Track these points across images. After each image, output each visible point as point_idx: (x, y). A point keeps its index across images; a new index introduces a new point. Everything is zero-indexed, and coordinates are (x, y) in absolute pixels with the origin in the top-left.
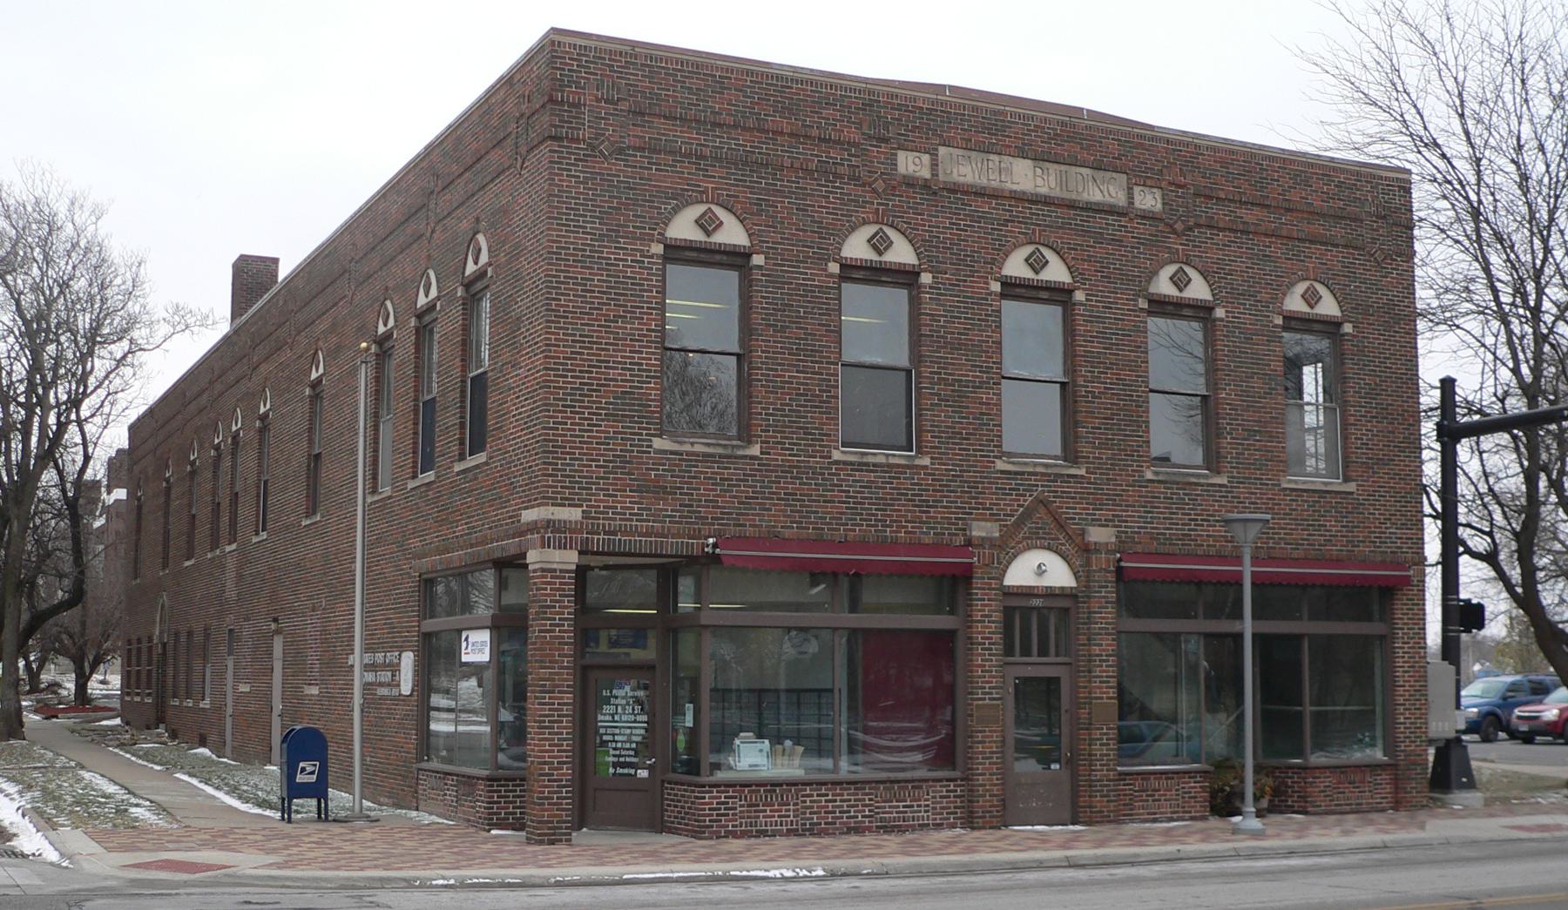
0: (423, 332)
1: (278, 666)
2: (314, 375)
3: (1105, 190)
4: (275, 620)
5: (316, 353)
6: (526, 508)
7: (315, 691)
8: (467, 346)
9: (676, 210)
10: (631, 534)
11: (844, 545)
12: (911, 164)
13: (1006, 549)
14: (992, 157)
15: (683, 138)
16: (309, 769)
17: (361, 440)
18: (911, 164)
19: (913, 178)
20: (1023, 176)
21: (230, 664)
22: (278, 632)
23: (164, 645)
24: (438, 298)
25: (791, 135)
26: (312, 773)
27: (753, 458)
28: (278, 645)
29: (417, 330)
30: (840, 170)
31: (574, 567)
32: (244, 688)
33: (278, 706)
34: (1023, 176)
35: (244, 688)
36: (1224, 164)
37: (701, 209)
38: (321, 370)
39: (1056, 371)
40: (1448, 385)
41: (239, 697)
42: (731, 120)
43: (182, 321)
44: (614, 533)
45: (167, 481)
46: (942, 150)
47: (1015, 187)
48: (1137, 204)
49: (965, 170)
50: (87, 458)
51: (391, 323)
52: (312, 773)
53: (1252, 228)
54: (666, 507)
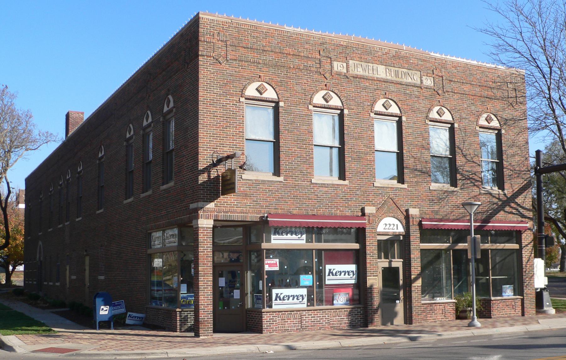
0: (145, 137)
1: (87, 268)
2: (100, 155)
3: (414, 78)
4: (86, 251)
5: (101, 147)
6: (192, 203)
7: (102, 278)
8: (164, 138)
9: (249, 84)
10: (234, 212)
11: (314, 216)
12: (339, 67)
13: (378, 218)
14: (370, 64)
15: (251, 56)
16: (106, 309)
17: (151, 145)
18: (339, 67)
19: (340, 73)
20: (381, 72)
21: (68, 268)
22: (87, 255)
23: (41, 262)
24: (152, 122)
25: (293, 55)
26: (106, 310)
27: (280, 182)
28: (87, 260)
29: (143, 135)
30: (312, 69)
31: (212, 226)
32: (74, 277)
33: (88, 284)
34: (381, 72)
35: (74, 277)
36: (455, 67)
37: (260, 83)
38: (103, 153)
39: (395, 148)
40: (538, 152)
41: (71, 281)
42: (269, 49)
43: (48, 137)
44: (227, 212)
45: (41, 199)
46: (351, 62)
47: (378, 76)
48: (424, 83)
49: (358, 68)
50: (9, 192)
51: (132, 133)
52: (106, 310)
53: (467, 93)
54: (248, 202)
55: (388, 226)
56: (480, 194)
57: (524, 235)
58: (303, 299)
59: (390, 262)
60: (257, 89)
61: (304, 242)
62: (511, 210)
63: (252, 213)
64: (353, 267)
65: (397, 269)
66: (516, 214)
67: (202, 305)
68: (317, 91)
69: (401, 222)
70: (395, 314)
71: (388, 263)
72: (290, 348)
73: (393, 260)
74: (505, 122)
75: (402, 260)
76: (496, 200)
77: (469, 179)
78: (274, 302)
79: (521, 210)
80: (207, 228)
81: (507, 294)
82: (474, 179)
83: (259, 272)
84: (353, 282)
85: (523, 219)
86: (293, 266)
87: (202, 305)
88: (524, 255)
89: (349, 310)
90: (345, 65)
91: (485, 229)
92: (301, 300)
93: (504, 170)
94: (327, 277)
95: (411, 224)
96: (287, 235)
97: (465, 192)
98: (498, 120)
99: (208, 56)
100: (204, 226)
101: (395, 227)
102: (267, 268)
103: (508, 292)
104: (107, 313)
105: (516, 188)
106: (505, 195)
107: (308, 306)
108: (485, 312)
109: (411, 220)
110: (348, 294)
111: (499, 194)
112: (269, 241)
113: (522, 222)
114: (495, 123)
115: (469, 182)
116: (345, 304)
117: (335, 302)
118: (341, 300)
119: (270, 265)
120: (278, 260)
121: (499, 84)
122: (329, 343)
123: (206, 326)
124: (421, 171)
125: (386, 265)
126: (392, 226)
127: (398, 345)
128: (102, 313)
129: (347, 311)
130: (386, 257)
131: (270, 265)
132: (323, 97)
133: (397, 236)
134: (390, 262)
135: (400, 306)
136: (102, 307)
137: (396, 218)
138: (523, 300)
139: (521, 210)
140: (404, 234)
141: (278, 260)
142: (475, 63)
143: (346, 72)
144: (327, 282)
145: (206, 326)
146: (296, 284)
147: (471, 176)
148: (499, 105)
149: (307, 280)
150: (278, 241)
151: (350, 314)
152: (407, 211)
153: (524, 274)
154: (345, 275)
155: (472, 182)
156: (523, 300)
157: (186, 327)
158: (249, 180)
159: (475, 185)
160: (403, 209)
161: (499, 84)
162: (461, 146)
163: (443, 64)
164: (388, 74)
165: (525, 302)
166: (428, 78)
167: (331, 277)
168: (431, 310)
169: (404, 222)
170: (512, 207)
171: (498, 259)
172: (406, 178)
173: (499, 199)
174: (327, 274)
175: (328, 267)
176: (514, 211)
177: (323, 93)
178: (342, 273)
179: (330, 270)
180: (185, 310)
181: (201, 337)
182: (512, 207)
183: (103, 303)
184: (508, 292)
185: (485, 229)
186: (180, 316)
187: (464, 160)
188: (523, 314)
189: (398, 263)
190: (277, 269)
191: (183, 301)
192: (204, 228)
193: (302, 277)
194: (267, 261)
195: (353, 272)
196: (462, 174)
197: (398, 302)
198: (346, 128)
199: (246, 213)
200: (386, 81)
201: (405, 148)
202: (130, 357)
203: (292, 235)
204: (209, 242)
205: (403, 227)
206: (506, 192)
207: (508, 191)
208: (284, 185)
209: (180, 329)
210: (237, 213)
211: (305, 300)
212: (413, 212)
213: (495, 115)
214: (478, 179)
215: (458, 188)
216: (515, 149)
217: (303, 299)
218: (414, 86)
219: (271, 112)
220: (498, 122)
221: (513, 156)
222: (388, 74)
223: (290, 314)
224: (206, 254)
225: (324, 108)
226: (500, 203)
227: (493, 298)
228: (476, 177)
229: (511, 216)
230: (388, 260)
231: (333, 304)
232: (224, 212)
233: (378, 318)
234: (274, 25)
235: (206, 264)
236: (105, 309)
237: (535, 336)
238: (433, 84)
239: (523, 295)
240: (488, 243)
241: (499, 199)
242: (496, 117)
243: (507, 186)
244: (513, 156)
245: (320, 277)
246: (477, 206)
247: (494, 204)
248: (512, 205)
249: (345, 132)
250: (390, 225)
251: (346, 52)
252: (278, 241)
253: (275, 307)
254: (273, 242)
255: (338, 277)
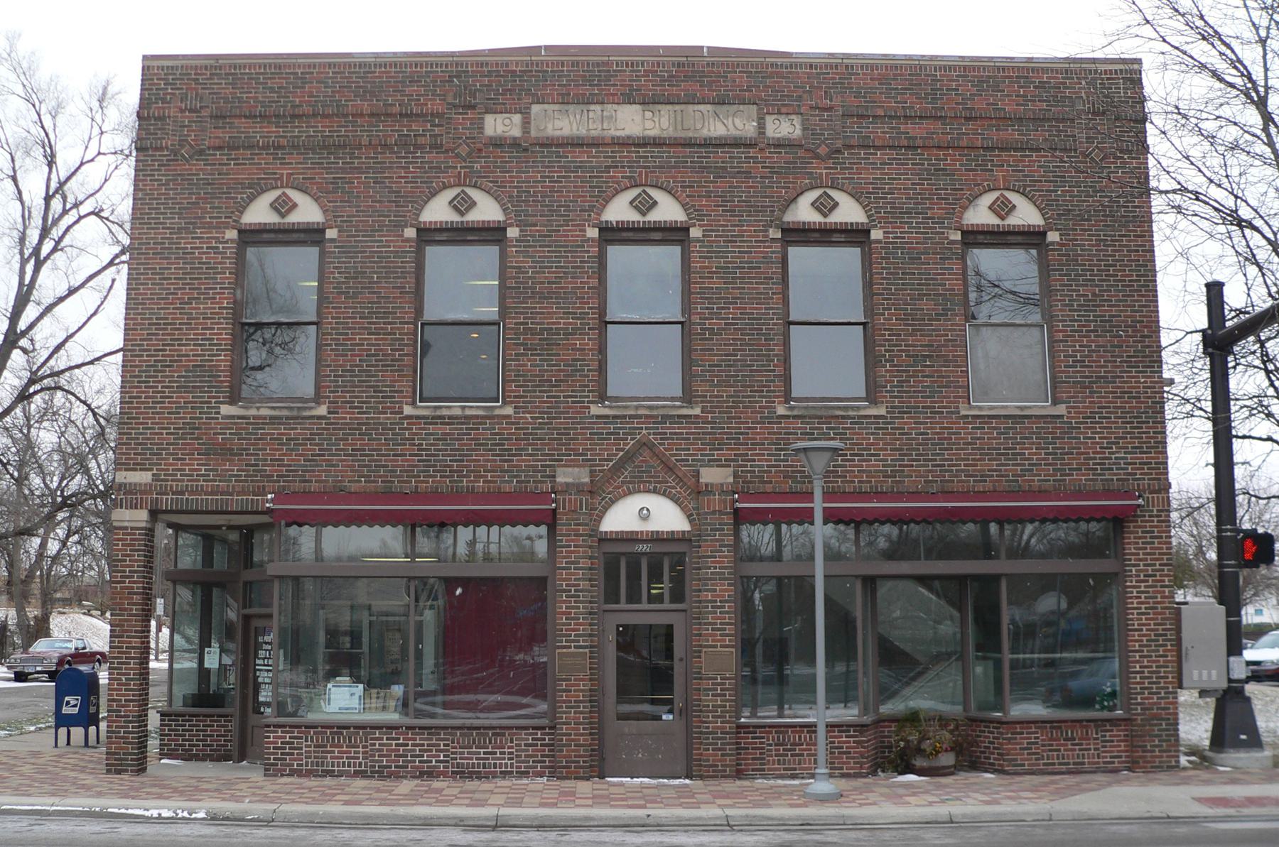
12: (498, 125)
16: (73, 703)
18: (498, 125)
20: (630, 121)
26: (75, 706)
34: (630, 121)
44: (182, 493)
52: (75, 706)
63: (242, 493)
80: (132, 528)
100: (126, 524)
127: (467, 801)
192: (126, 528)
202: (53, 829)
204: (136, 561)
224: (127, 588)
235: (125, 610)
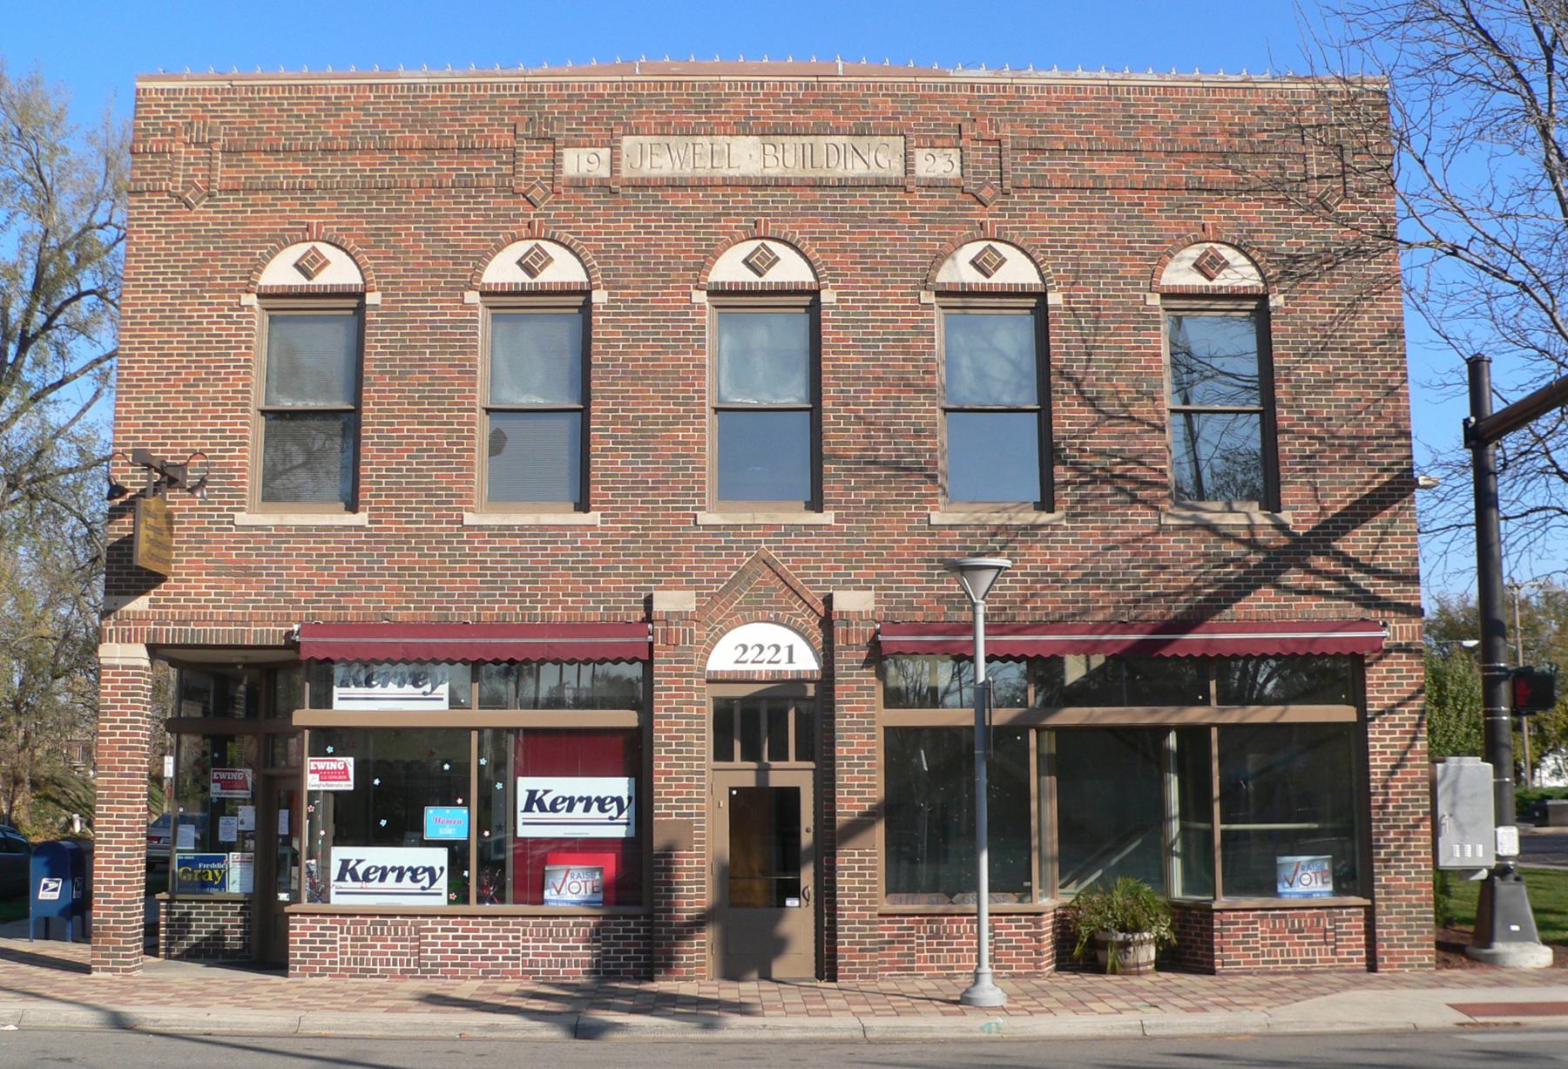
9: (272, 254)
14: (699, 139)
18: (580, 162)
20: (746, 156)
26: (55, 890)
27: (361, 528)
34: (746, 156)
44: (185, 622)
47: (731, 173)
52: (55, 890)
55: (752, 654)
56: (1161, 529)
57: (1374, 675)
58: (433, 880)
59: (763, 771)
60: (296, 266)
61: (444, 705)
62: (1310, 580)
64: (619, 786)
65: (793, 794)
66: (1338, 596)
67: (101, 882)
68: (499, 248)
69: (807, 639)
70: (779, 946)
71: (753, 773)
72: (119, 1022)
73: (774, 764)
74: (1290, 269)
75: (811, 765)
76: (1233, 550)
77: (1110, 479)
78: (335, 886)
79: (1363, 581)
81: (1300, 888)
82: (1133, 479)
83: (278, 791)
84: (620, 832)
85: (1372, 614)
86: (396, 785)
87: (101, 882)
88: (1375, 746)
89: (592, 921)
90: (605, 153)
91: (1167, 653)
92: (426, 883)
93: (1280, 439)
94: (522, 817)
95: (839, 643)
96: (384, 686)
97: (1092, 528)
98: (1255, 263)
99: (154, 192)
100: (116, 662)
101: (784, 653)
102: (312, 782)
103: (1307, 879)
104: (56, 896)
105: (1338, 500)
106: (1281, 527)
107: (450, 902)
108: (1189, 951)
109: (839, 630)
110: (601, 870)
111: (1251, 527)
112: (323, 700)
113: (1363, 623)
114: (1240, 274)
115: (1108, 490)
116: (587, 903)
117: (547, 894)
118: (571, 887)
119: (325, 775)
120: (350, 760)
121: (1265, 136)
122: (258, 1019)
123: (110, 942)
124: (896, 466)
125: (748, 780)
126: (768, 654)
128: (43, 895)
129: (588, 925)
130: (751, 753)
131: (325, 775)
132: (519, 262)
133: (798, 682)
134: (763, 771)
135: (798, 917)
136: (45, 881)
137: (787, 626)
138: (1370, 913)
139: (1363, 581)
140: (817, 676)
141: (350, 760)
142: (1149, 78)
143: (607, 174)
144: (523, 832)
145: (110, 942)
146: (406, 831)
147: (1118, 470)
148: (1254, 212)
149: (448, 821)
150: (352, 703)
151: (596, 935)
152: (828, 601)
153: (1375, 814)
154: (587, 809)
155: (1121, 490)
156: (1370, 913)
157: (185, 945)
158: (257, 527)
159: (1135, 500)
160: (815, 595)
161: (1265, 136)
162: (1077, 369)
163: (1011, 102)
164: (771, 161)
165: (1382, 920)
166: (936, 152)
167: (536, 814)
168: (936, 936)
169: (818, 635)
170: (1317, 573)
171: (1252, 762)
172: (831, 490)
173: (1253, 544)
174: (521, 804)
175: (525, 784)
176: (1324, 584)
177: (520, 248)
178: (574, 806)
179: (532, 793)
180: (179, 897)
181: (95, 974)
182: (1317, 573)
183: (45, 870)
184: (1307, 879)
185: (1167, 653)
186: (168, 913)
187: (1086, 413)
188: (1372, 967)
189: (793, 774)
190: (348, 785)
191: (186, 872)
192: (117, 667)
193: (431, 813)
194: (311, 763)
195: (619, 800)
196: (1075, 466)
197: (791, 902)
198: (597, 346)
199: (243, 623)
200: (763, 184)
201: (830, 391)
203: (400, 685)
205: (816, 654)
206: (1286, 516)
207: (1297, 514)
208: (374, 538)
209: (168, 950)
210: (217, 623)
211: (442, 882)
212: (846, 601)
213: (1237, 248)
214: (1149, 476)
215: (1058, 514)
216: (1332, 361)
217: (433, 880)
218: (879, 184)
219: (803, 320)
220: (1253, 270)
221: (1328, 383)
222: (771, 161)
223: (379, 923)
225: (523, 293)
226: (1255, 558)
227: (1221, 901)
228: (1140, 472)
229: (1312, 605)
230: (753, 765)
231: (542, 902)
232: (177, 623)
233: (700, 951)
234: (557, 70)
235: (116, 768)
236: (52, 885)
237: (168, 1030)
238: (957, 170)
239: (1369, 893)
240: (1206, 702)
241: (1253, 544)
242: (1246, 255)
243: (1290, 494)
244: (1328, 383)
245: (493, 811)
246: (991, 575)
247: (1227, 562)
248: (1319, 562)
249: (596, 360)
250: (763, 648)
251: (607, 117)
252: (352, 703)
253: (336, 900)
254: (337, 705)
255: (563, 815)
